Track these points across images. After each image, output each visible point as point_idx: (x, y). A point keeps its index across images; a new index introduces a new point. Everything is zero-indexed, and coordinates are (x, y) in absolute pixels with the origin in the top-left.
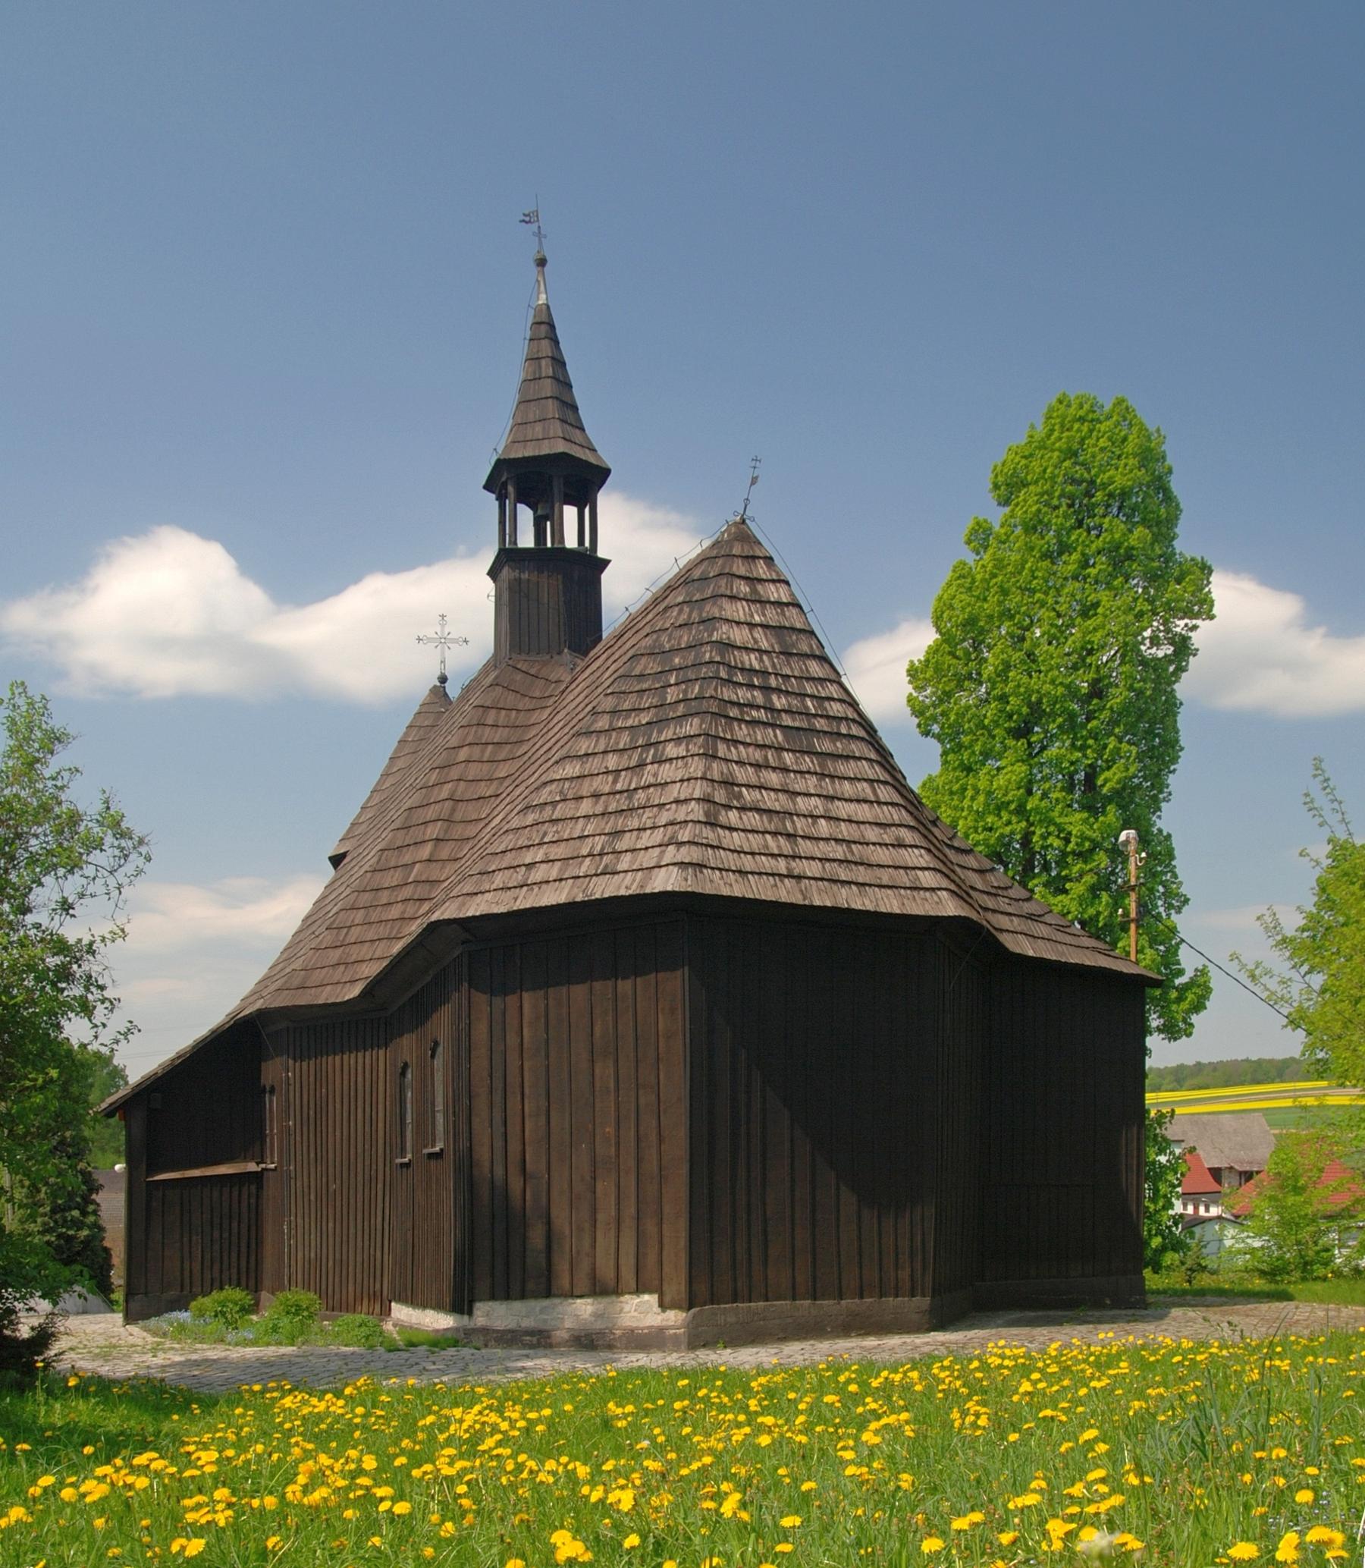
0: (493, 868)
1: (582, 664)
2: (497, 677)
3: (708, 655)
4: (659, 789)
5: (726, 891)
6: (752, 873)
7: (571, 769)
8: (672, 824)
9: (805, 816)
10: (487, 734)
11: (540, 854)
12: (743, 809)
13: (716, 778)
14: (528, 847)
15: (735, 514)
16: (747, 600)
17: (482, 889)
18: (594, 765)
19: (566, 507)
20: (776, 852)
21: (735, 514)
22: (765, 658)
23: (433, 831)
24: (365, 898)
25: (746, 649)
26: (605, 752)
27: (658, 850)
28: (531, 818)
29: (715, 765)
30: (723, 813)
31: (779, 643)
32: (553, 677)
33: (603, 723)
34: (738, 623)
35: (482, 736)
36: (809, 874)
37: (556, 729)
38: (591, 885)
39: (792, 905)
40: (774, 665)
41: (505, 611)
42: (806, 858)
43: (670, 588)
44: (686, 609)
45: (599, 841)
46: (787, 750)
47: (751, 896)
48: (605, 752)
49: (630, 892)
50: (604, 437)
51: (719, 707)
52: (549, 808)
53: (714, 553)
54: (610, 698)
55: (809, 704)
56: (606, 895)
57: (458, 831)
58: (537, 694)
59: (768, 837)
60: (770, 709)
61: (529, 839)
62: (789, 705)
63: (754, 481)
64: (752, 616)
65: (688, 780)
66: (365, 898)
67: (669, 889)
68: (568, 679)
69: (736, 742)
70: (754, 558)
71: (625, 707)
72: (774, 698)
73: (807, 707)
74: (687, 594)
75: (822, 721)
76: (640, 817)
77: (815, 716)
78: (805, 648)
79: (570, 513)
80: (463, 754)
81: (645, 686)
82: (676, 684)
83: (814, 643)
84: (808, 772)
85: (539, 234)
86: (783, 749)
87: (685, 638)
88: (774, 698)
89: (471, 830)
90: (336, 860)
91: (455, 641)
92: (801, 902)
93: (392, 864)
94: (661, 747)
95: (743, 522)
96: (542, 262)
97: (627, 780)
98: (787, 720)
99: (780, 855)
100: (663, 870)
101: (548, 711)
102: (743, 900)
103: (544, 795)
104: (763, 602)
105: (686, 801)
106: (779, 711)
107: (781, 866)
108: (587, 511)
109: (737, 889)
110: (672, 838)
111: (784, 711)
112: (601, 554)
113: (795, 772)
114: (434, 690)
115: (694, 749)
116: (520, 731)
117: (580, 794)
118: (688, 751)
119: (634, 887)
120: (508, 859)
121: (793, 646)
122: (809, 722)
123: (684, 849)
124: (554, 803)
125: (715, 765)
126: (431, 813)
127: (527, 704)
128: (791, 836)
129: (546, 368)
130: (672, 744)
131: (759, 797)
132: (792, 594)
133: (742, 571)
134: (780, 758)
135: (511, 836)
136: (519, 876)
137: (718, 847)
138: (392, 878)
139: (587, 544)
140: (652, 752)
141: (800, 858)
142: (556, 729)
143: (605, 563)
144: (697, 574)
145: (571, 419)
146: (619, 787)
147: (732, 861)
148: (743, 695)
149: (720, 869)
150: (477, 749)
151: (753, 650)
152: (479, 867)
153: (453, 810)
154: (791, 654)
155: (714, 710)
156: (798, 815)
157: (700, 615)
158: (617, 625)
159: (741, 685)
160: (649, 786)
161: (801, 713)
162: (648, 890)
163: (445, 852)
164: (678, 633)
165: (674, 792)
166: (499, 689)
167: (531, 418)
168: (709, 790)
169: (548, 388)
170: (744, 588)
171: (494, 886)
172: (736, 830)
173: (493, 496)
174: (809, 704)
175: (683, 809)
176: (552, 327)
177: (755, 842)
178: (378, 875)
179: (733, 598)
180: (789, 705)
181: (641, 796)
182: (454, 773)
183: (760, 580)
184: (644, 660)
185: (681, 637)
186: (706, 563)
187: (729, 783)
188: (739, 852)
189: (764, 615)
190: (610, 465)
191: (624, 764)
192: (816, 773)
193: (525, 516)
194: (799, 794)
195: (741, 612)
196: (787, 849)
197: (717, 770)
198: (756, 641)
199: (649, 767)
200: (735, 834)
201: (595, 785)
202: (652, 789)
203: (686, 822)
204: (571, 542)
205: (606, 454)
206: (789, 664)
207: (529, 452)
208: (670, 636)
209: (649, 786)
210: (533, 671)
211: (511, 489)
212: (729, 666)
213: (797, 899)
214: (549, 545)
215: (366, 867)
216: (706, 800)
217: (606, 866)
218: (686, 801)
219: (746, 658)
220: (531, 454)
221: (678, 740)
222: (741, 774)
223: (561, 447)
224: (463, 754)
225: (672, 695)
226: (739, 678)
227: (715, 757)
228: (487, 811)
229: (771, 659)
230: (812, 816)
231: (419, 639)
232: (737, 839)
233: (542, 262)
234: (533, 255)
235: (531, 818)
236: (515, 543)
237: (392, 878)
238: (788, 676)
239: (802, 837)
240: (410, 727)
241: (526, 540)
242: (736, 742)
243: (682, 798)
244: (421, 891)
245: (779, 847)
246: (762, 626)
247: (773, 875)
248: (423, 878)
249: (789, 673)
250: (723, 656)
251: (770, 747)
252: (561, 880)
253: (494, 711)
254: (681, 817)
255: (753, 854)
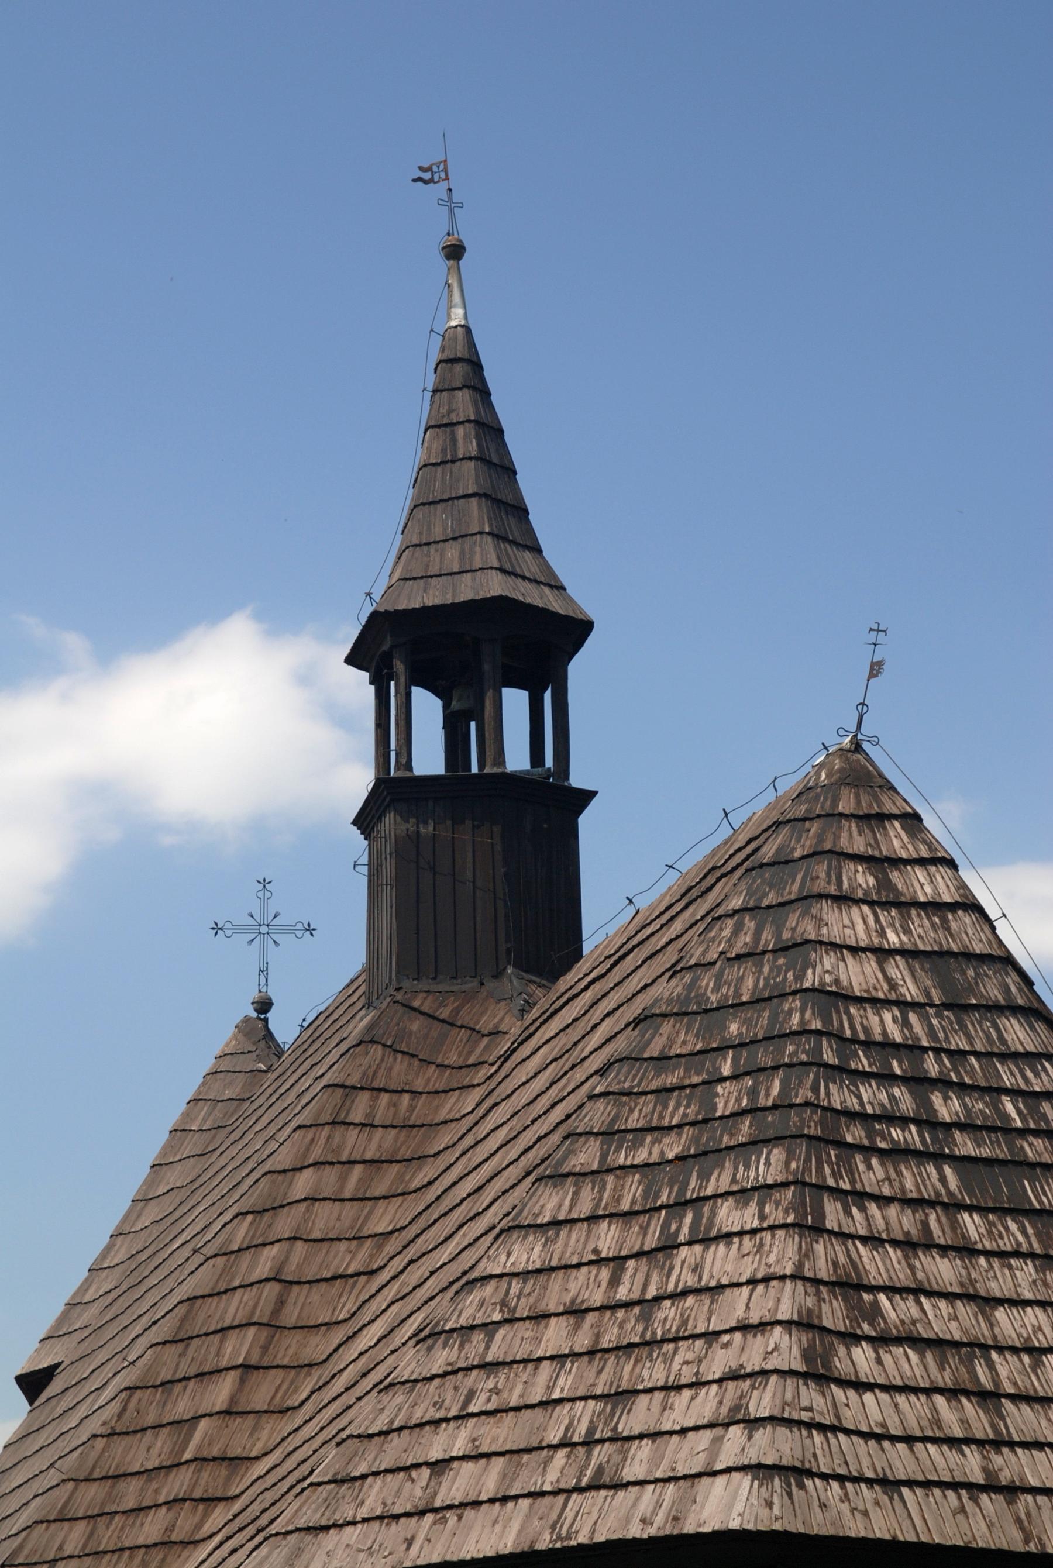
0: (362, 1469)
1: (543, 1003)
2: (370, 1027)
3: (796, 1019)
4: (706, 1299)
5: (855, 1528)
6: (910, 1484)
7: (526, 1253)
8: (734, 1376)
9: (1015, 1350)
10: (352, 1143)
11: (459, 1440)
12: (883, 1340)
13: (823, 1275)
14: (436, 1423)
15: (840, 731)
16: (871, 904)
17: (339, 1518)
18: (571, 1245)
19: (506, 692)
20: (958, 1432)
21: (840, 731)
22: (912, 1017)
23: (238, 1348)
24: (91, 1496)
25: (874, 1001)
26: (593, 1219)
27: (707, 1435)
28: (441, 1358)
29: (819, 1248)
30: (842, 1350)
31: (941, 987)
32: (485, 1024)
33: (587, 1156)
34: (855, 950)
35: (341, 1147)
36: (1034, 1482)
37: (492, 1143)
38: (569, 1513)
39: (1000, 1553)
40: (932, 1033)
41: (388, 896)
42: (1025, 1445)
43: (714, 873)
44: (750, 924)
45: (585, 1413)
46: (970, 1209)
47: (911, 1537)
48: (593, 1219)
49: (652, 1531)
50: (581, 556)
51: (822, 1122)
52: (478, 1337)
53: (802, 810)
54: (600, 1104)
55: (1010, 1108)
56: (600, 1538)
57: (290, 1348)
58: (453, 1058)
59: (940, 1400)
60: (929, 1123)
61: (438, 1405)
62: (968, 1111)
63: (875, 669)
64: (882, 934)
65: (766, 1280)
66: (91, 1496)
67: (734, 1525)
68: (515, 1031)
69: (861, 1197)
70: (883, 817)
71: (631, 1124)
72: (937, 1099)
73: (1006, 1117)
74: (750, 894)
75: (1039, 1143)
76: (668, 1360)
77: (1023, 1132)
78: (992, 992)
79: (515, 703)
80: (303, 1184)
81: (671, 1080)
82: (734, 1077)
83: (1012, 981)
84: (1017, 1254)
85: (450, 201)
86: (961, 1207)
87: (750, 983)
88: (937, 1099)
89: (317, 1346)
90: (33, 1384)
91: (288, 929)
92: (1020, 1548)
93: (150, 1419)
94: (706, 1209)
95: (857, 747)
96: (455, 252)
97: (640, 1278)
98: (965, 1145)
99: (968, 1441)
100: (721, 1480)
101: (476, 1094)
102: (893, 1547)
103: (471, 1309)
104: (905, 906)
105: (763, 1326)
106: (948, 1126)
107: (972, 1465)
108: (548, 696)
109: (878, 1520)
110: (735, 1408)
111: (962, 1126)
112: (577, 780)
113: (988, 1254)
114: (245, 1027)
115: (775, 1215)
116: (419, 1134)
117: (542, 1307)
118: (762, 1217)
119: (659, 1519)
120: (393, 1452)
121: (971, 990)
122: (1011, 1146)
123: (762, 1435)
124: (489, 1328)
125: (819, 1248)
126: (233, 1309)
127: (427, 1079)
128: (989, 1398)
129: (467, 442)
130: (731, 1201)
131: (915, 1312)
132: (963, 886)
133: (859, 844)
134: (955, 1225)
135: (400, 1398)
136: (413, 1491)
137: (834, 1429)
138: (152, 1451)
139: (549, 762)
140: (689, 1219)
141: (1012, 1444)
142: (492, 1143)
143: (587, 796)
144: (768, 852)
145: (515, 534)
146: (622, 1293)
147: (865, 1458)
148: (871, 1096)
149: (841, 1479)
150: (330, 1175)
151: (887, 1003)
152: (330, 1462)
153: (281, 1303)
154: (967, 1008)
155: (813, 1130)
156: (1000, 1349)
157: (778, 934)
158: (612, 929)
159: (866, 1076)
160: (685, 1293)
161: (993, 1129)
162: (689, 1528)
163: (263, 1392)
164: (733, 972)
165: (736, 1306)
166: (377, 1051)
167: (438, 533)
168: (810, 1302)
169: (469, 477)
170: (864, 879)
171: (363, 1512)
172: (870, 1387)
173: (365, 676)
174: (1010, 1108)
175: (758, 1344)
176: (475, 365)
177: (912, 1412)
178: (120, 1444)
179: (843, 900)
180: (968, 1111)
181: (668, 1314)
182: (284, 1224)
183: (897, 862)
184: (667, 1027)
185: (741, 979)
186: (785, 830)
187: (849, 1285)
188: (879, 1438)
189: (907, 931)
190: (592, 614)
191: (633, 1244)
192: (1032, 1255)
193: (427, 709)
194: (1000, 1302)
195: (860, 928)
196: (980, 1423)
197: (824, 1257)
198: (893, 986)
199: (684, 1251)
200: (868, 1397)
201: (573, 1287)
202: (690, 1300)
203: (764, 1373)
204: (517, 758)
205: (585, 592)
206: (963, 1028)
207: (434, 596)
208: (719, 977)
209: (685, 1293)
210: (444, 1013)
211: (399, 667)
212: (841, 1038)
213: (1010, 1539)
214: (475, 769)
215: (94, 1425)
216: (804, 1323)
217: (600, 1470)
218: (763, 1326)
219: (874, 1020)
220: (438, 601)
221: (741, 1195)
222: (878, 1265)
223: (495, 586)
224: (303, 1184)
225: (727, 1098)
226: (863, 1062)
227: (819, 1230)
228: (351, 1306)
229: (925, 1019)
230: (1030, 1350)
231: (217, 929)
232: (874, 1409)
233: (455, 252)
234: (438, 239)
235: (441, 1358)
236: (409, 767)
237: (152, 1451)
238: (963, 1053)
239: (1012, 1397)
240: (194, 1101)
241: (429, 758)
242: (861, 1197)
243: (755, 1320)
244: (209, 1481)
245: (964, 1422)
246: (903, 952)
247: (954, 1486)
248: (215, 1452)
249: (964, 1046)
250: (826, 1019)
251: (932, 1204)
252: (504, 1499)
253: (365, 1096)
254: (753, 1363)
255: (909, 1440)
